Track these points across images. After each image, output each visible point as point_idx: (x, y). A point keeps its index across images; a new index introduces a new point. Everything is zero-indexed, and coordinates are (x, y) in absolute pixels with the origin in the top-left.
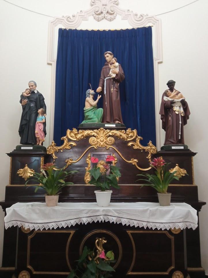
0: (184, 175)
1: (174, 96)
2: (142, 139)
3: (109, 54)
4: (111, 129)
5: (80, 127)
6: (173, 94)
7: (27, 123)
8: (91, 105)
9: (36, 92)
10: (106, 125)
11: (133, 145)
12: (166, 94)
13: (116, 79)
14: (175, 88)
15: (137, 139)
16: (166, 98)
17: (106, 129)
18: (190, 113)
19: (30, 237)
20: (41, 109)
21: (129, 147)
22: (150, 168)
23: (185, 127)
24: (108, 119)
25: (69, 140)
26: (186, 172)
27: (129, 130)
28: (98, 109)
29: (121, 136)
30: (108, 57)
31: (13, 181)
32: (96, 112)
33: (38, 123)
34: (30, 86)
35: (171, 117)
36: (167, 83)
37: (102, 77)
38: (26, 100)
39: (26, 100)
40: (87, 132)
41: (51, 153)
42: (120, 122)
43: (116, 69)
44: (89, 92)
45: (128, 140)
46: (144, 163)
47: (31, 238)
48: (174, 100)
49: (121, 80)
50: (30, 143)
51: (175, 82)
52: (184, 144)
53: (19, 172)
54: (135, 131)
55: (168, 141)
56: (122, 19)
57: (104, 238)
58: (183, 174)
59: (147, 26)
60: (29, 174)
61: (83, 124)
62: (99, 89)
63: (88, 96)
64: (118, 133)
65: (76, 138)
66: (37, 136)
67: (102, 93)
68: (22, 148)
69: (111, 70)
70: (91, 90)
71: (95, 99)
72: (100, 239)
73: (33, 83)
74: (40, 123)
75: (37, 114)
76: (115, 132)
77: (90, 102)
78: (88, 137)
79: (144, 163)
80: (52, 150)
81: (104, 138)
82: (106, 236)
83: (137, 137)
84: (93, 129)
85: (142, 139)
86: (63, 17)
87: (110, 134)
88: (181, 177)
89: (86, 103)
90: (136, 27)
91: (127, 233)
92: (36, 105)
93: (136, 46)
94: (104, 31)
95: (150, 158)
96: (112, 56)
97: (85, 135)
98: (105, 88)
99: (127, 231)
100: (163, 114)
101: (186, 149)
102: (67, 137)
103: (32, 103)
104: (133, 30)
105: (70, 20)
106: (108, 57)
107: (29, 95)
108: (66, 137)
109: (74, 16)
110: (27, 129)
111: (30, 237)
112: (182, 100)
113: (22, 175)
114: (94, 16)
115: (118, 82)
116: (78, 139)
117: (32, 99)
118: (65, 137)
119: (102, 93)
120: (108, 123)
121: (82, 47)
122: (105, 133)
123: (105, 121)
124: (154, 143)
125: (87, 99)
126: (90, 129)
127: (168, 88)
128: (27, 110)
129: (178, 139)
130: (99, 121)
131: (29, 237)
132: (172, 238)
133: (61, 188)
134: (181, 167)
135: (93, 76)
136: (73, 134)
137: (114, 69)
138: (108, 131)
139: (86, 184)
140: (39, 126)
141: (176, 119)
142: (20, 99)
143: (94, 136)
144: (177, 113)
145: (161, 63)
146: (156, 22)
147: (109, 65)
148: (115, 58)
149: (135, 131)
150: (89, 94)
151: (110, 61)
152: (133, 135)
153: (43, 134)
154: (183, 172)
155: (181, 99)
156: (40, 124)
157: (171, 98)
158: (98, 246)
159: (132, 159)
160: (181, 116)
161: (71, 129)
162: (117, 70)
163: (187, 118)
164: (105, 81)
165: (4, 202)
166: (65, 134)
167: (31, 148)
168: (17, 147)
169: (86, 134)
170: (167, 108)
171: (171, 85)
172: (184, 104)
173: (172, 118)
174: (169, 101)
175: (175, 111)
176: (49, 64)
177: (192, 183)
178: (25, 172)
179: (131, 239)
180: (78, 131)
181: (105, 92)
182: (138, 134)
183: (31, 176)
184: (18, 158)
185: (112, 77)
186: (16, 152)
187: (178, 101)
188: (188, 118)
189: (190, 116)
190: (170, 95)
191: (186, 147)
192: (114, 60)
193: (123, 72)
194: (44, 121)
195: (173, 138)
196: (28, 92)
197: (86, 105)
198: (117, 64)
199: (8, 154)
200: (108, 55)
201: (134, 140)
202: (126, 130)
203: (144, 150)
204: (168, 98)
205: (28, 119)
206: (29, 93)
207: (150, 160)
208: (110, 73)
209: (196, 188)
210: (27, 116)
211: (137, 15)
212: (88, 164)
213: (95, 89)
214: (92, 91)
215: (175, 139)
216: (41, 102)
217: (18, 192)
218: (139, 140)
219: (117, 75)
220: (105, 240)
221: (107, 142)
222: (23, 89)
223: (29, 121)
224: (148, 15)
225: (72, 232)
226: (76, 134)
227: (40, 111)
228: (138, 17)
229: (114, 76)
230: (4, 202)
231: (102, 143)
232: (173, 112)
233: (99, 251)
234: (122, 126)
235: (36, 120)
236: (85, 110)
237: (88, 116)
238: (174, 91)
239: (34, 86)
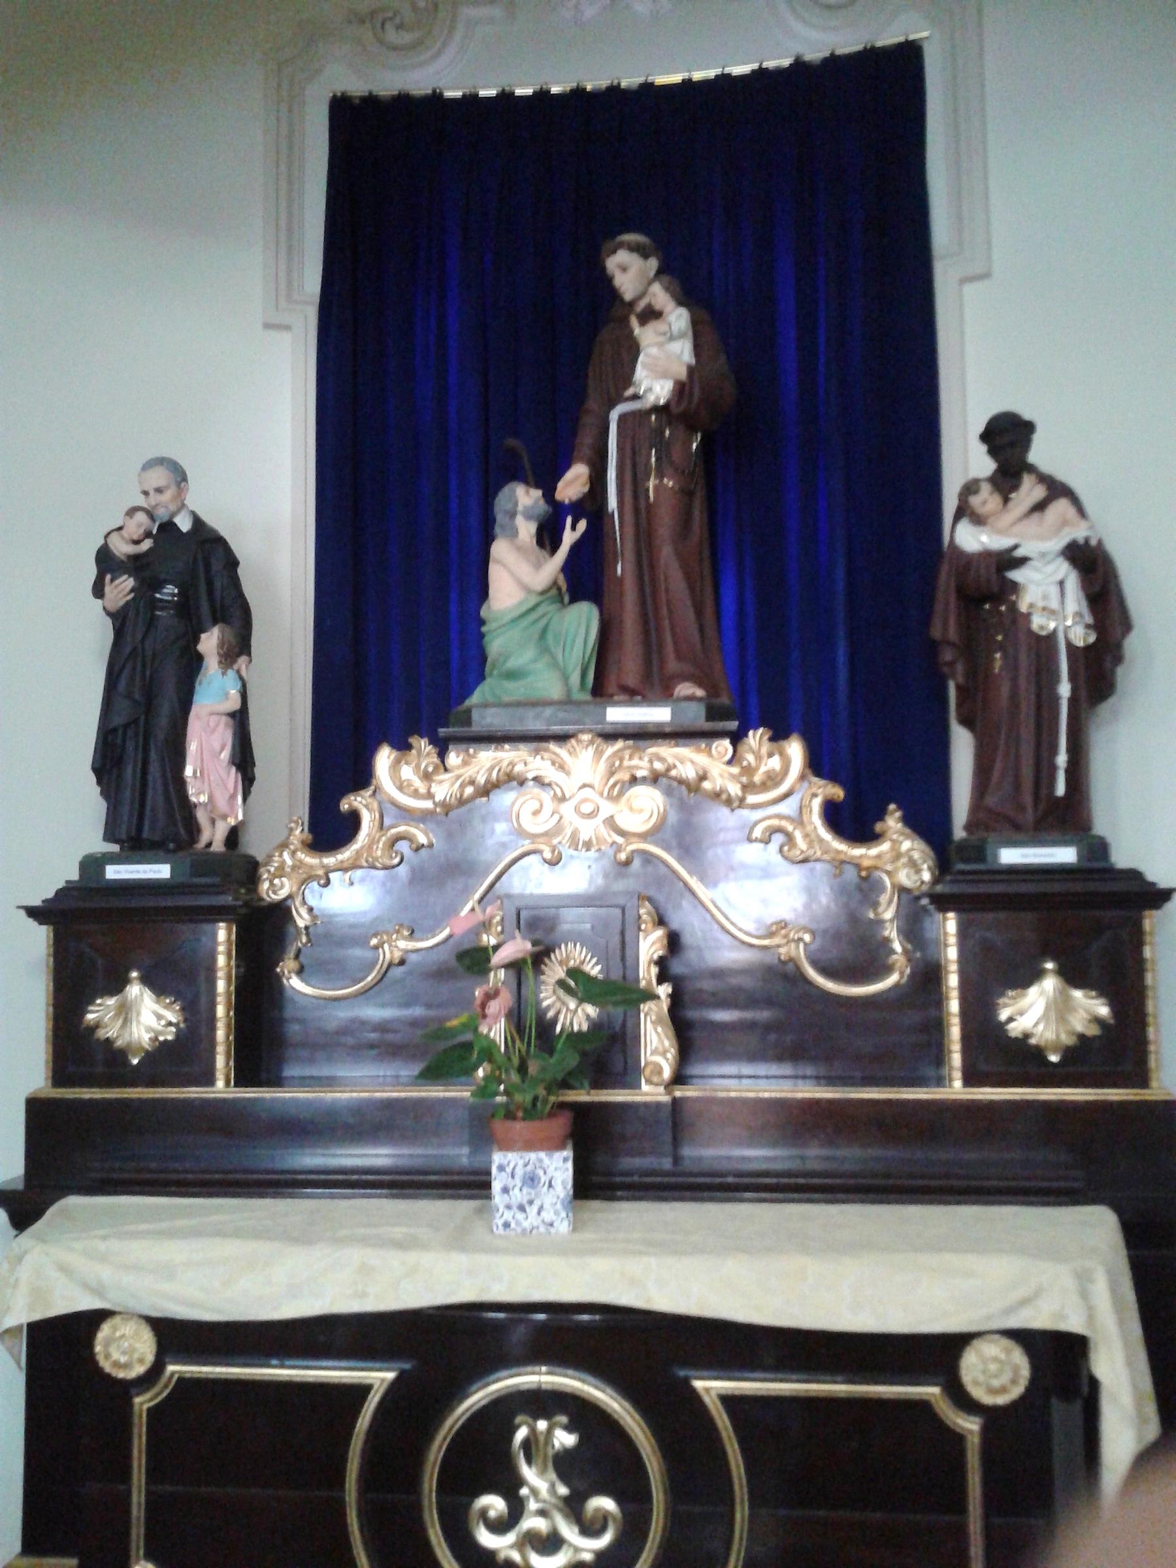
4: (641, 735)
7: (136, 721)
19: (142, 1402)
24: (629, 665)
30: (624, 269)
31: (61, 1073)
32: (554, 623)
35: (1005, 657)
36: (980, 427)
37: (592, 404)
39: (127, 583)
41: (283, 894)
47: (149, 1410)
53: (93, 1012)
57: (563, 1419)
62: (573, 483)
65: (430, 796)
67: (591, 506)
68: (114, 872)
72: (542, 1425)
77: (517, 572)
82: (581, 1413)
85: (837, 792)
91: (694, 1395)
96: (653, 264)
99: (698, 1384)
103: (174, 591)
110: (136, 749)
111: (142, 1404)
115: (692, 428)
119: (591, 506)
120: (633, 695)
123: (612, 687)
129: (1044, 792)
131: (137, 1400)
132: (970, 1425)
133: (891, 932)
134: (1073, 976)
135: (548, 379)
136: (407, 772)
142: (92, 572)
147: (634, 321)
154: (1090, 1008)
158: (529, 1462)
160: (1069, 645)
165: (20, 1186)
166: (362, 778)
167: (161, 871)
171: (1008, 436)
172: (1092, 565)
173: (1012, 665)
177: (1141, 1079)
178: (125, 1012)
179: (724, 1435)
180: (442, 755)
184: (91, 936)
191: (1097, 849)
192: (659, 296)
198: (678, 318)
206: (148, 534)
213: (547, 482)
217: (96, 1138)
220: (569, 1428)
222: (111, 509)
230: (20, 1186)
233: (535, 1492)
238: (1028, 481)
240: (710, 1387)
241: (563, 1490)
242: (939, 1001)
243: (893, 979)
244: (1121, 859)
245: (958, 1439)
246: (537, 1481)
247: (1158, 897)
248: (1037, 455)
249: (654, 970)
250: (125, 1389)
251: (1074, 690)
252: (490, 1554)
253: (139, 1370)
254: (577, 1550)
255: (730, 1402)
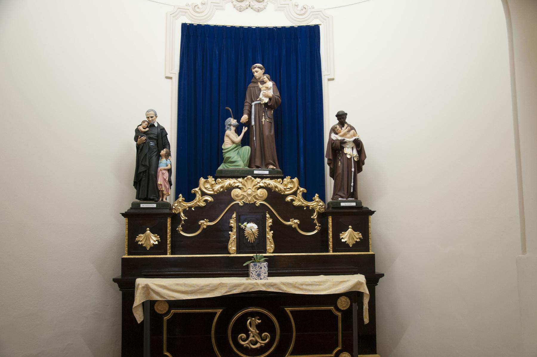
0: (358, 240)
1: (344, 135)
2: (305, 191)
3: (259, 68)
4: (262, 177)
5: (216, 175)
6: (344, 130)
7: (146, 171)
8: (233, 142)
9: (156, 125)
10: (256, 172)
11: (292, 200)
12: (334, 130)
13: (269, 104)
14: (346, 121)
15: (299, 191)
16: (334, 137)
17: (255, 178)
18: (366, 157)
20: (165, 150)
21: (288, 202)
22: (316, 232)
23: (359, 175)
24: (258, 162)
25: (203, 194)
26: (361, 236)
27: (287, 180)
28: (242, 146)
29: (276, 187)
30: (257, 72)
33: (161, 170)
34: (148, 118)
37: (248, 100)
38: (144, 138)
39: (144, 138)
40: (228, 182)
42: (275, 168)
43: (269, 91)
44: (229, 123)
45: (287, 193)
46: (307, 225)
48: (344, 139)
49: (275, 106)
50: (152, 198)
51: (346, 114)
52: (357, 199)
54: (295, 180)
55: (337, 195)
56: (276, 10)
58: (357, 239)
59: (312, 23)
60: (152, 242)
61: (221, 171)
63: (228, 128)
64: (272, 183)
65: (213, 190)
66: (159, 188)
69: (262, 92)
70: (232, 119)
71: (238, 131)
73: (152, 112)
74: (165, 170)
75: (159, 157)
76: (268, 181)
77: (231, 137)
78: (230, 188)
79: (307, 225)
80: (179, 207)
81: (249, 186)
83: (298, 189)
84: (237, 177)
85: (305, 191)
86: (187, 5)
87: (262, 185)
88: (355, 242)
89: (226, 139)
90: (296, 24)
92: (157, 145)
93: (295, 52)
94: (250, 28)
95: (316, 217)
97: (225, 186)
98: (253, 117)
100: (331, 157)
101: (359, 207)
102: (200, 189)
103: (150, 141)
104: (292, 28)
105: (198, 10)
106: (257, 72)
107: (147, 129)
108: (199, 188)
109: (203, 4)
110: (144, 179)
112: (355, 139)
113: (143, 242)
114: (234, 3)
116: (216, 191)
117: (152, 136)
118: (197, 189)
119: (248, 124)
120: (258, 167)
121: (217, 53)
122: (253, 184)
124: (323, 197)
125: (228, 132)
126: (232, 177)
127: (337, 122)
128: (146, 150)
130: (245, 165)
132: (339, 314)
134: (355, 229)
136: (208, 186)
137: (267, 90)
138: (258, 180)
139: (230, 254)
140: (163, 174)
141: (349, 163)
142: (134, 134)
143: (237, 187)
144: (349, 157)
145: (333, 79)
146: (325, 19)
148: (267, 75)
149: (295, 180)
150: (230, 125)
151: (259, 78)
152: (292, 186)
153: (168, 186)
154: (357, 236)
155: (354, 138)
156: (164, 172)
157: (341, 136)
159: (291, 220)
160: (354, 160)
161: (206, 178)
162: (270, 93)
163: (361, 164)
164: (253, 107)
166: (197, 185)
167: (155, 206)
168: (133, 204)
169: (226, 184)
170: (337, 148)
171: (341, 117)
172: (358, 144)
173: (343, 164)
174: (337, 140)
175: (346, 154)
176: (167, 78)
178: (148, 238)
180: (215, 180)
181: (253, 123)
182: (301, 185)
183: (155, 243)
184: (136, 220)
185: (263, 102)
186: (133, 211)
187: (350, 141)
188: (363, 164)
189: (366, 161)
190: (340, 133)
191: (359, 203)
192: (265, 78)
193: (278, 94)
194: (169, 167)
195: (344, 191)
196: (145, 125)
197: (225, 141)
198: (270, 84)
199: (123, 215)
200: (257, 69)
201: (295, 193)
202: (283, 178)
203: (308, 207)
204: (337, 136)
205: (147, 164)
206: (147, 127)
207: (316, 221)
208: (261, 96)
209: (373, 256)
210: (146, 161)
211: (297, 6)
212: (231, 227)
214: (233, 121)
215: (346, 192)
216: (163, 138)
218: (301, 194)
219: (270, 99)
221: (257, 197)
222: (138, 119)
223: (149, 168)
224: (313, 8)
225: (219, 311)
226: (212, 185)
227: (163, 152)
228: (299, 8)
229: (266, 100)
231: (250, 198)
232: (344, 155)
233: (252, 332)
234: (278, 172)
235: (157, 166)
236: (225, 149)
237: (229, 158)
238: (346, 126)
239: (155, 117)
240: (288, 310)
241: (258, 332)
242: (328, 234)
243: (316, 232)
244: (364, 205)
245: (337, 317)
246: (253, 330)
247: (372, 213)
248: (347, 120)
249: (269, 228)
250: (161, 316)
251: (355, 170)
252: (243, 345)
253: (165, 312)
254: (261, 343)
255: (291, 312)
